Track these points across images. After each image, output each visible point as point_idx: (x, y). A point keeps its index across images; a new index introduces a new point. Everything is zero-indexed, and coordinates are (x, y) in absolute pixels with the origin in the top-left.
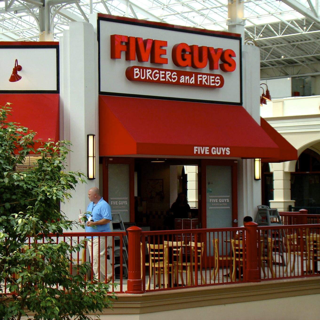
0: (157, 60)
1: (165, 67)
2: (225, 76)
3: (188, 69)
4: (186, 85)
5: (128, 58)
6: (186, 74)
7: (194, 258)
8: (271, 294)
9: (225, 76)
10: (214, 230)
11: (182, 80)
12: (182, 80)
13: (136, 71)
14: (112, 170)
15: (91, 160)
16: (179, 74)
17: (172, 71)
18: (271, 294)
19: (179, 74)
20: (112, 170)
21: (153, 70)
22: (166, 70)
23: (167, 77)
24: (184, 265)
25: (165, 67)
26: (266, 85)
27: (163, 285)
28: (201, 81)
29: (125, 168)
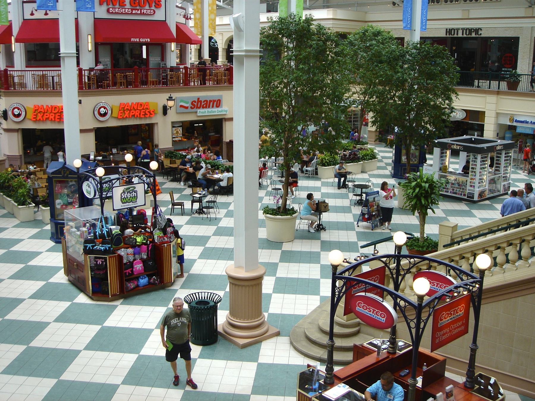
0: (121, 4)
1: (126, 7)
2: (156, 10)
3: (138, 8)
4: (136, 14)
5: (108, 5)
6: (135, 10)
7: (198, 104)
8: (516, 291)
9: (156, 10)
10: (152, 69)
11: (134, 12)
12: (134, 12)
13: (111, 9)
14: (101, 49)
15: (89, 44)
16: (132, 10)
17: (128, 9)
18: (516, 291)
19: (132, 10)
20: (101, 49)
21: (119, 8)
22: (125, 9)
23: (126, 11)
24: (110, 66)
25: (126, 7)
26: (342, 377)
27: (442, 191)
28: (143, 12)
29: (108, 48)
